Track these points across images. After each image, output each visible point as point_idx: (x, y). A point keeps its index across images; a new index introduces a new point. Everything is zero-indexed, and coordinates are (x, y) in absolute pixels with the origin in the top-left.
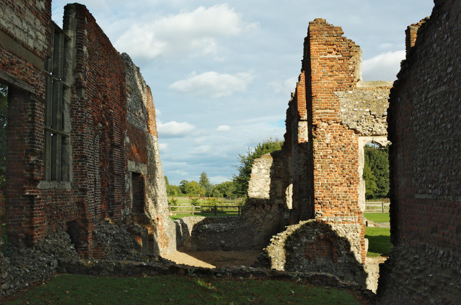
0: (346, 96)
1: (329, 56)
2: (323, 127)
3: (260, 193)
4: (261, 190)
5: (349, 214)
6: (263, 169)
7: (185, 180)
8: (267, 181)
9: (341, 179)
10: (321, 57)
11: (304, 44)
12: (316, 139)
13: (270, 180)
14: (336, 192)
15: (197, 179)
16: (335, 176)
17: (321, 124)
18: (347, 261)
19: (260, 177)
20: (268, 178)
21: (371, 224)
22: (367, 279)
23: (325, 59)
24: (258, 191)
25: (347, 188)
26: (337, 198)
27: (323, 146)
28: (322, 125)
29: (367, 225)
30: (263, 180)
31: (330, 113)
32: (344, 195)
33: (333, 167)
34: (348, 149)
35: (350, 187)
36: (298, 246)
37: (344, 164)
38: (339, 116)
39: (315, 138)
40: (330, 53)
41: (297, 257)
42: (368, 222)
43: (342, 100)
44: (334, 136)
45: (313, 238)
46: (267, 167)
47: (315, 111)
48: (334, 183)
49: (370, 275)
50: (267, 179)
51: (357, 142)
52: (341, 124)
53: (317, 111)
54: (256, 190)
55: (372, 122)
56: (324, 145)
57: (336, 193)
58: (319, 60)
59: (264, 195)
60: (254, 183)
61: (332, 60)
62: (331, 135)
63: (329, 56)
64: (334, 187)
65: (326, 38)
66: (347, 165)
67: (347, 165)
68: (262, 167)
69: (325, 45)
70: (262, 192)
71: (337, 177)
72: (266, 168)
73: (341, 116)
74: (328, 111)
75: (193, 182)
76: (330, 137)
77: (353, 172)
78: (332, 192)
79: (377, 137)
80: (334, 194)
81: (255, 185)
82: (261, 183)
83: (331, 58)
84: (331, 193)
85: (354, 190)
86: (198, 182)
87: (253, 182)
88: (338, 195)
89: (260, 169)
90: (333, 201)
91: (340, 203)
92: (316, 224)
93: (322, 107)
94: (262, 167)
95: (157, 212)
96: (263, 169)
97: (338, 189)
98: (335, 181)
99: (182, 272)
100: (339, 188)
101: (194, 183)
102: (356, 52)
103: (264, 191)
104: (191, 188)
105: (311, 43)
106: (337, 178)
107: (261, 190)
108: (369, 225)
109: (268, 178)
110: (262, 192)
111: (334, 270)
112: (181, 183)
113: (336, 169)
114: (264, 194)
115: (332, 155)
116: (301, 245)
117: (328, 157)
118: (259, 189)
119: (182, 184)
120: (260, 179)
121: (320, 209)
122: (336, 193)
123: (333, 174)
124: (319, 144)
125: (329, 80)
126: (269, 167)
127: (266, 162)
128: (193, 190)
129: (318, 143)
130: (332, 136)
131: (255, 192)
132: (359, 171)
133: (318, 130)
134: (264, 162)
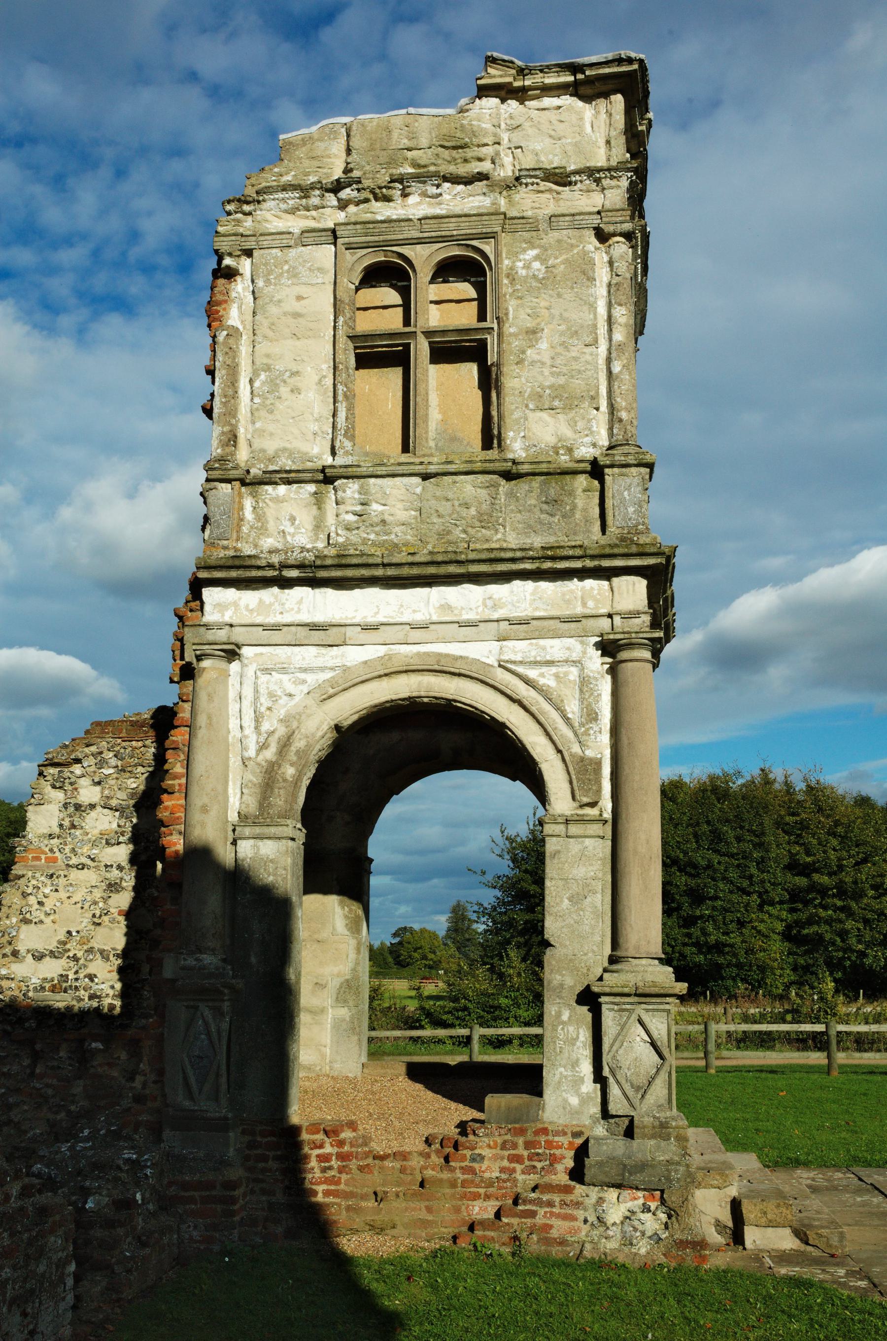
3: (63, 962)
4: (74, 948)
6: (92, 806)
7: (408, 926)
8: (113, 887)
13: (129, 880)
15: (440, 924)
19: (74, 861)
20: (120, 868)
21: (771, 1224)
24: (53, 955)
29: (737, 1237)
30: (90, 877)
42: (749, 1211)
46: (122, 795)
50: (115, 873)
54: (40, 947)
59: (91, 977)
60: (32, 900)
68: (88, 793)
70: (75, 959)
72: (114, 803)
75: (423, 931)
81: (38, 915)
82: (77, 897)
86: (442, 933)
87: (25, 895)
89: (78, 807)
94: (88, 793)
96: (92, 806)
101: (426, 935)
103: (90, 950)
104: (415, 950)
107: (74, 948)
108: (752, 1236)
109: (120, 868)
110: (75, 959)
112: (395, 935)
114: (92, 969)
118: (62, 936)
119: (396, 940)
120: (74, 874)
126: (132, 796)
127: (113, 762)
128: (425, 957)
131: (39, 957)
134: (102, 764)
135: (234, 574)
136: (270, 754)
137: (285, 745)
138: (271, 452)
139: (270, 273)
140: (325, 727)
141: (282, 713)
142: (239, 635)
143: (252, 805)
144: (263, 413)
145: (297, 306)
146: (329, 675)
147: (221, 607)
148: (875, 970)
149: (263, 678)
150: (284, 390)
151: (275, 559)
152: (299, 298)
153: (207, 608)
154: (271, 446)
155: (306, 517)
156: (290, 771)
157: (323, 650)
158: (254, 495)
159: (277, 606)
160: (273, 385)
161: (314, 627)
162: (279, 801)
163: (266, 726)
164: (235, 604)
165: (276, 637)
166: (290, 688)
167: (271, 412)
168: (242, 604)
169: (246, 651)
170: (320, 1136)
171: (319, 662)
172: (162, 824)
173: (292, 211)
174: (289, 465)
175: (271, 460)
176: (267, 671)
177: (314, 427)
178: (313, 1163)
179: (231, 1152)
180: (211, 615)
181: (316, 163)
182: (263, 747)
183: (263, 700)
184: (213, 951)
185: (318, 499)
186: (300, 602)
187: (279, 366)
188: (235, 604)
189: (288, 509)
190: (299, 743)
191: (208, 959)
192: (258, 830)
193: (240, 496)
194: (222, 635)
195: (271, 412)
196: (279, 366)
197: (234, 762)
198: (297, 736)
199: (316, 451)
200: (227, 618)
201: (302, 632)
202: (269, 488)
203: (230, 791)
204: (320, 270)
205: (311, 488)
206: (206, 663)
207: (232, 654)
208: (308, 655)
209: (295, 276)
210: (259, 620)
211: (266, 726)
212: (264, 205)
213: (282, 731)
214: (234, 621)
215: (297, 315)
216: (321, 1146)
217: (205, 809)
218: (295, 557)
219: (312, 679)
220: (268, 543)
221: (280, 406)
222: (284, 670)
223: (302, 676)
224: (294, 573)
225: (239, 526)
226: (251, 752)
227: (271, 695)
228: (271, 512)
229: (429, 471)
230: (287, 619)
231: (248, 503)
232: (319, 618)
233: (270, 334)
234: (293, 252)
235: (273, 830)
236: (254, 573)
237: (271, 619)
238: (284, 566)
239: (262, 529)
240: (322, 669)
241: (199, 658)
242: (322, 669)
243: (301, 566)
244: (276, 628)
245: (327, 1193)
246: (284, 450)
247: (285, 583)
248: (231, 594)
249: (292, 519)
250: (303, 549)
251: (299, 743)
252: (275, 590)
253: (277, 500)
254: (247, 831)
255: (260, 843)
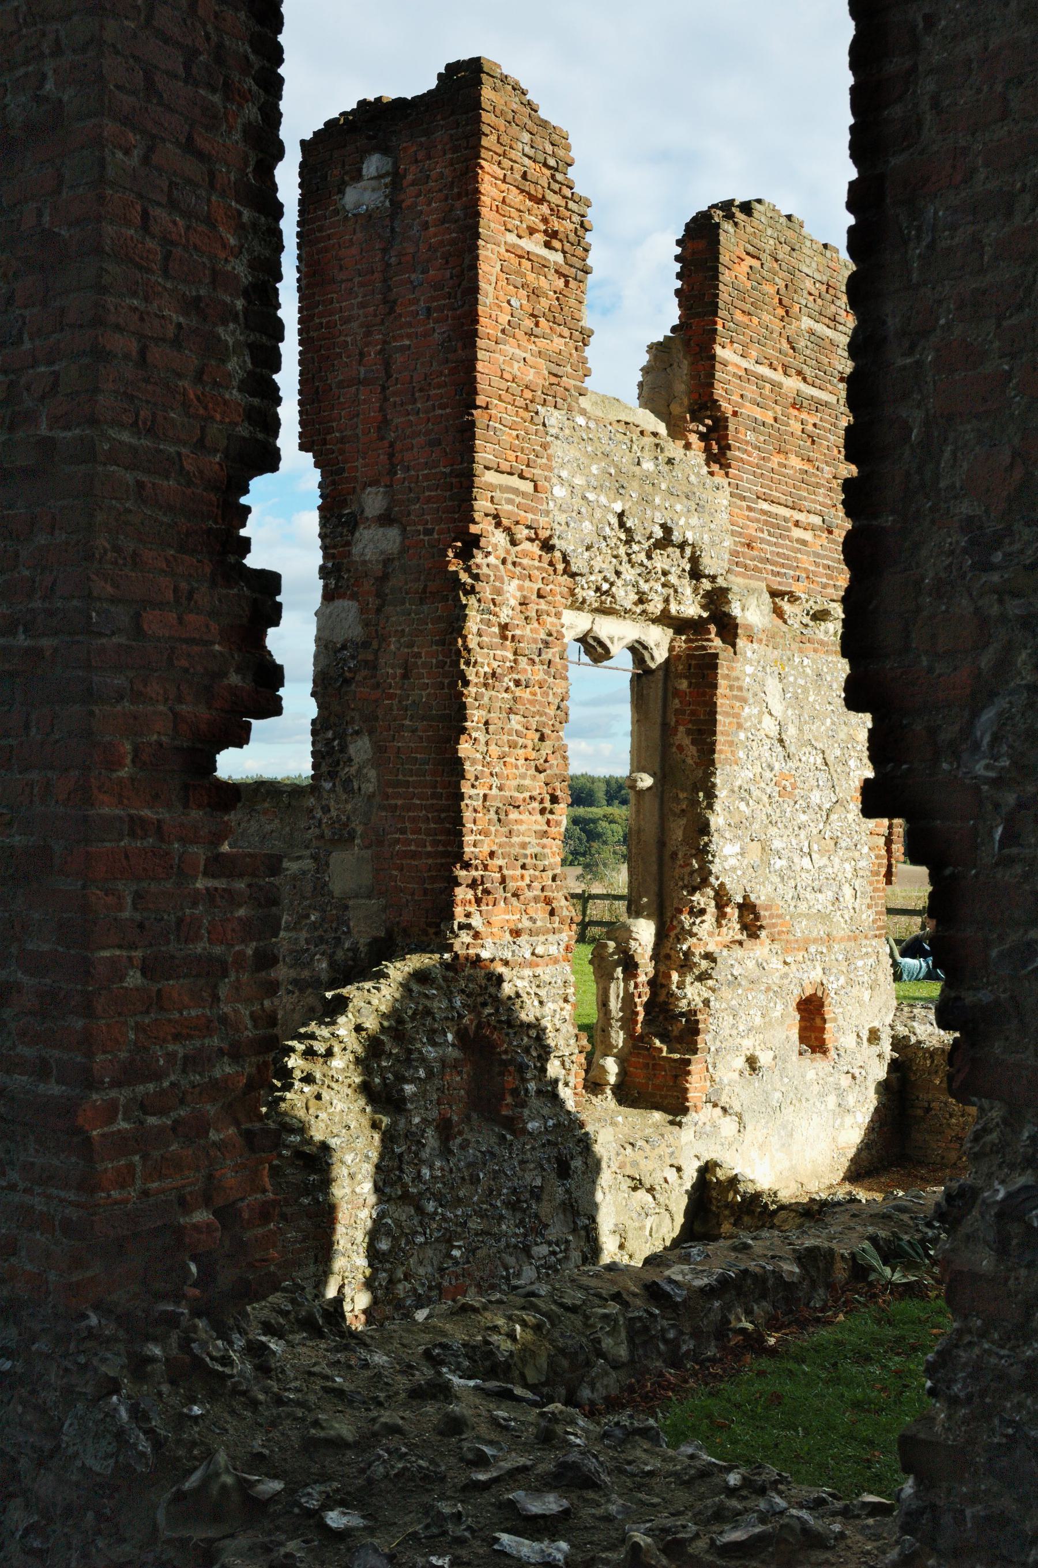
11: (852, 156)
12: (472, 601)
18: (550, 1123)
23: (519, 253)
25: (539, 817)
35: (550, 817)
36: (419, 1078)
38: (547, 513)
39: (472, 591)
41: (414, 1129)
44: (525, 597)
52: (542, 548)
55: (616, 557)
65: (526, 161)
74: (514, 481)
83: (538, 256)
92: (454, 966)
93: (505, 466)
95: (709, 1521)
105: (483, 163)
115: (516, 677)
116: (430, 1074)
121: (473, 908)
124: (481, 621)
125: (409, 336)
129: (479, 617)
133: (479, 558)
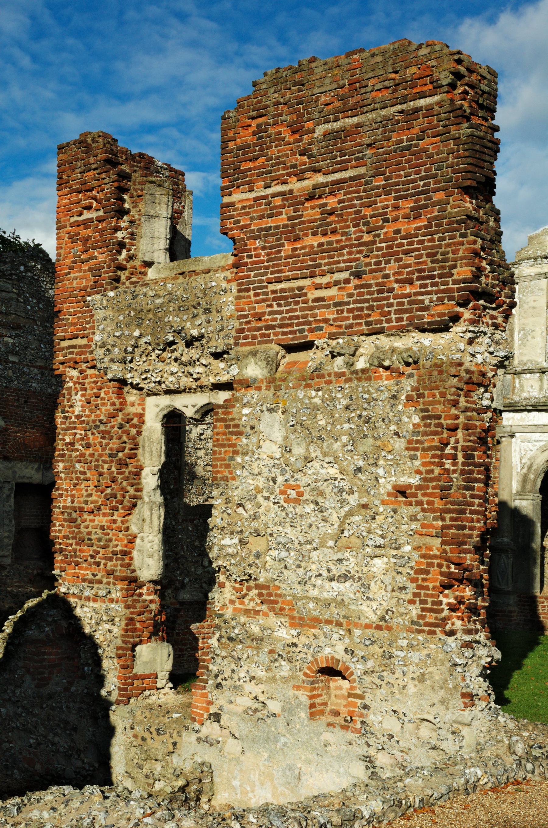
0: (105, 304)
1: (87, 215)
2: (71, 378)
5: (105, 580)
9: (96, 498)
10: (72, 220)
14: (87, 527)
16: (87, 491)
17: (69, 372)
22: (114, 741)
26: (87, 541)
27: (70, 423)
28: (70, 374)
31: (80, 347)
32: (101, 535)
33: (82, 469)
34: (113, 427)
37: (101, 462)
40: (89, 208)
43: (100, 314)
45: (47, 629)
47: (59, 344)
48: (84, 505)
49: (119, 731)
51: (144, 409)
53: (64, 344)
56: (73, 419)
57: (86, 530)
58: (68, 228)
61: (86, 224)
62: (82, 396)
63: (87, 215)
64: (86, 516)
66: (106, 466)
67: (106, 466)
69: (80, 192)
71: (90, 492)
73: (95, 353)
76: (81, 401)
77: (119, 481)
78: (78, 527)
79: (178, 396)
80: (82, 533)
84: (76, 530)
85: (119, 524)
88: (89, 533)
90: (78, 548)
91: (91, 553)
97: (93, 521)
98: (86, 502)
99: (11, 647)
100: (97, 518)
102: (139, 196)
106: (91, 495)
111: (65, 709)
113: (88, 475)
117: (77, 446)
122: (86, 530)
123: (83, 486)
130: (83, 399)
132: (145, 479)
135: (511, 408)
136: (525, 471)
137: (530, 467)
138: (525, 361)
139: (524, 292)
140: (543, 461)
141: (529, 456)
142: (514, 429)
143: (520, 489)
144: (522, 346)
145: (534, 304)
146: (543, 443)
147: (508, 419)
148: (54, 545)
149: (523, 444)
150: (529, 337)
151: (524, 403)
152: (534, 301)
153: (504, 420)
154: (525, 359)
155: (537, 385)
156: (532, 477)
157: (542, 434)
158: (519, 378)
159: (527, 419)
160: (526, 336)
161: (539, 426)
162: (528, 487)
163: (523, 461)
164: (513, 418)
165: (526, 430)
166: (531, 448)
167: (525, 346)
168: (515, 418)
169: (517, 434)
170: (543, 600)
171: (541, 439)
172: (215, 572)
173: (532, 266)
174: (531, 366)
175: (525, 364)
176: (523, 442)
177: (539, 351)
178: (540, 608)
179: (512, 601)
180: (505, 422)
181: (540, 245)
182: (522, 468)
183: (522, 452)
184: (507, 537)
185: (541, 379)
186: (534, 417)
187: (528, 328)
188: (513, 418)
189: (531, 382)
190: (535, 467)
191: (505, 540)
192: (521, 497)
193: (514, 379)
194: (508, 429)
195: (525, 346)
196: (528, 328)
197: (514, 473)
198: (534, 464)
199: (540, 360)
200: (510, 424)
201: (535, 428)
202: (524, 375)
203: (513, 483)
204: (542, 289)
205: (538, 375)
206: (503, 439)
207: (512, 436)
208: (537, 436)
209: (533, 292)
210: (521, 424)
211: (523, 461)
212: (522, 265)
213: (529, 463)
214: (513, 424)
215: (534, 308)
216: (543, 603)
217: (503, 490)
218: (533, 401)
219: (538, 444)
220: (525, 395)
221: (528, 344)
222: (529, 441)
223: (535, 443)
224: (530, 408)
225: (514, 390)
226: (519, 470)
227: (525, 450)
228: (525, 383)
229: (400, 483)
230: (530, 423)
231: (517, 381)
232: (540, 423)
233: (524, 315)
234: (532, 283)
235: (526, 497)
236: (517, 408)
237: (525, 424)
238: (527, 406)
239: (522, 390)
240: (542, 441)
241: (501, 437)
242: (542, 441)
243: (532, 406)
244: (526, 426)
245: (544, 618)
246: (529, 360)
247: (529, 411)
248: (511, 414)
249: (532, 386)
250: (535, 398)
251: (535, 467)
252: (526, 413)
253: (527, 379)
254: (518, 497)
255: (522, 501)
